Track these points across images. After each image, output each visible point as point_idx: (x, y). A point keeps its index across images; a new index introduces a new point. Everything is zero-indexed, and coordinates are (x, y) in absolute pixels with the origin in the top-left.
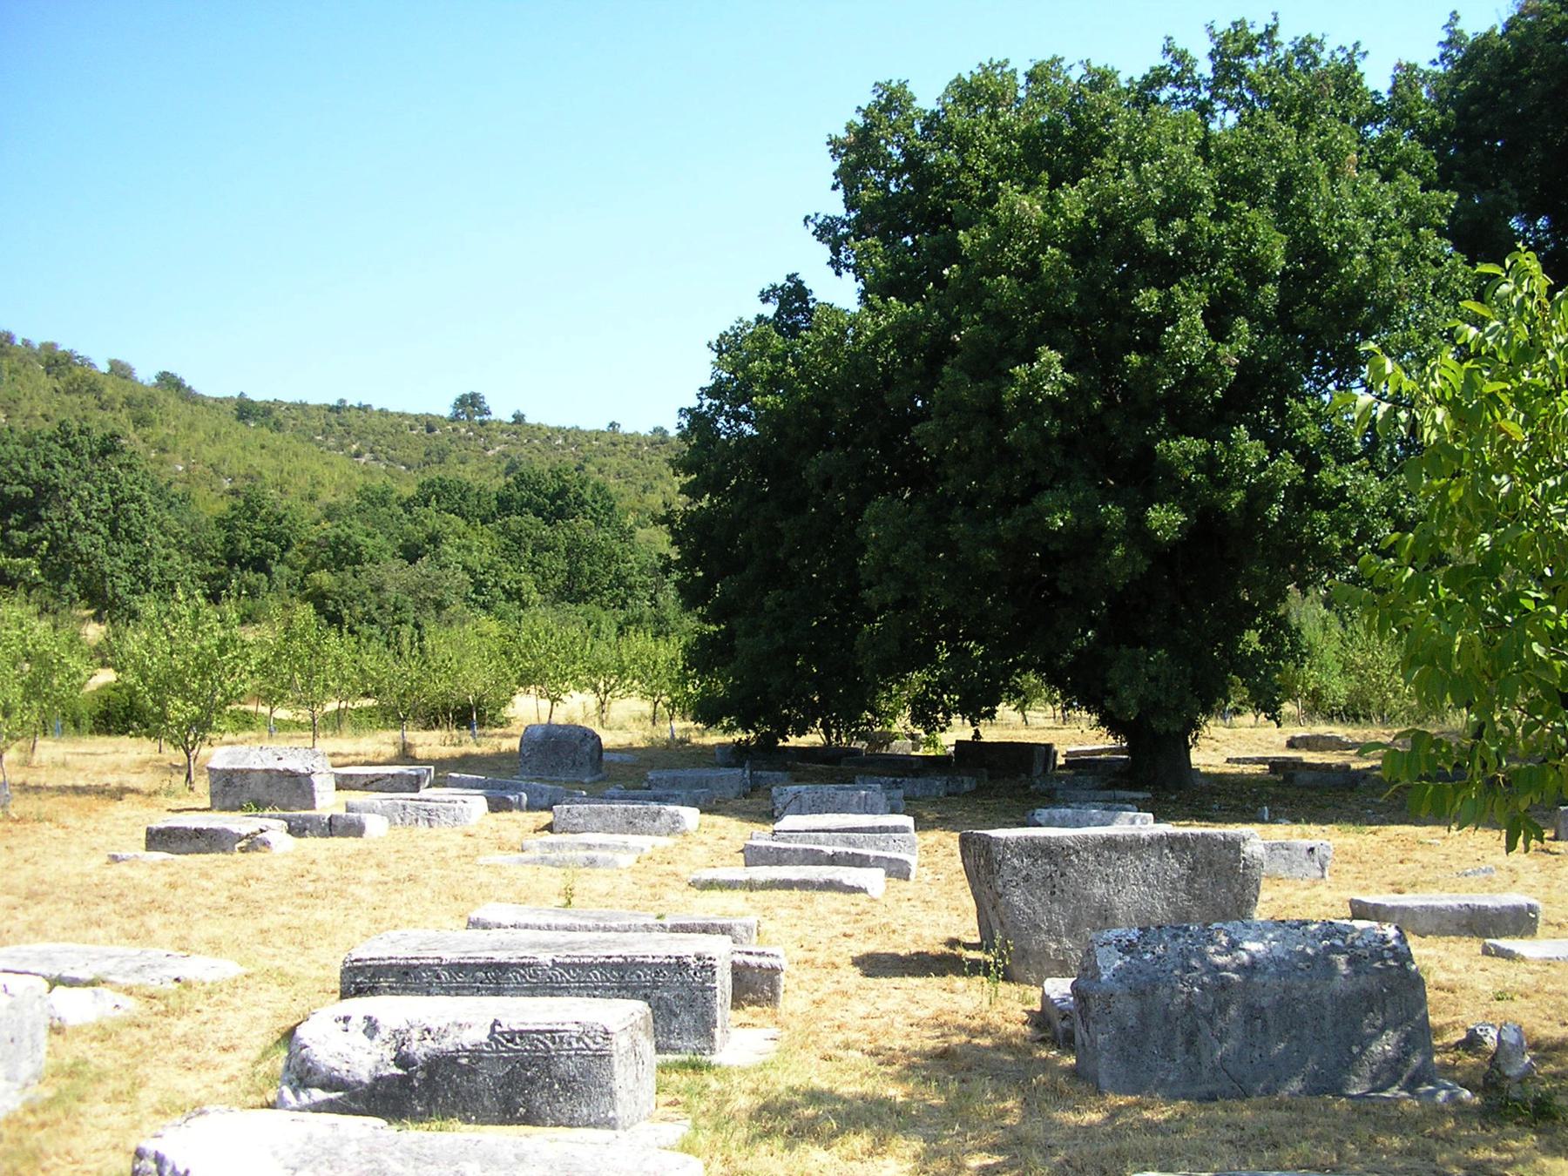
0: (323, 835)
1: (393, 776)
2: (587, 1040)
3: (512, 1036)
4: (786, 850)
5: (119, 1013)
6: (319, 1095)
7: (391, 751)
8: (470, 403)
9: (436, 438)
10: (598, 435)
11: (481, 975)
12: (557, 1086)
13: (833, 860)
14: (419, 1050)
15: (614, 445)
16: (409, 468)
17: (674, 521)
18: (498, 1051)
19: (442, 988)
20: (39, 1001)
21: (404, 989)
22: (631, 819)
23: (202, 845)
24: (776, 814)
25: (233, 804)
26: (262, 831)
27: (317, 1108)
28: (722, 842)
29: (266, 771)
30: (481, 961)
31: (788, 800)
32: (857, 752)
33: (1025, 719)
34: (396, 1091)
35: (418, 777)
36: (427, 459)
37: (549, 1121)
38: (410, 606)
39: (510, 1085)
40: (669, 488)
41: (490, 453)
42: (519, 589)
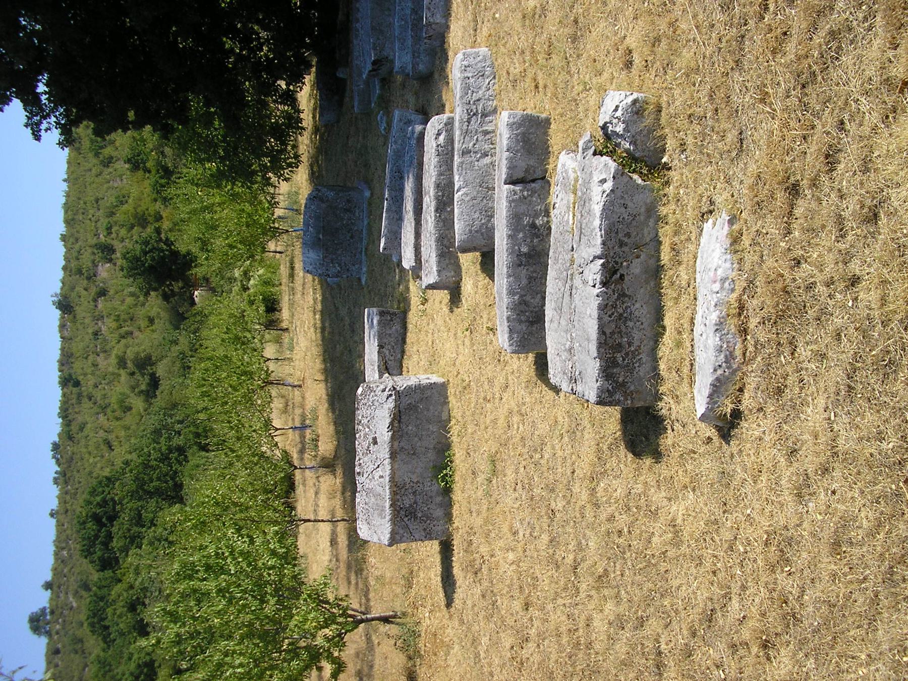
1: (381, 346)
7: (331, 482)
8: (37, 623)
9: (64, 647)
10: (60, 525)
15: (67, 511)
25: (441, 505)
29: (393, 455)
36: (80, 653)
40: (99, 465)
41: (75, 604)
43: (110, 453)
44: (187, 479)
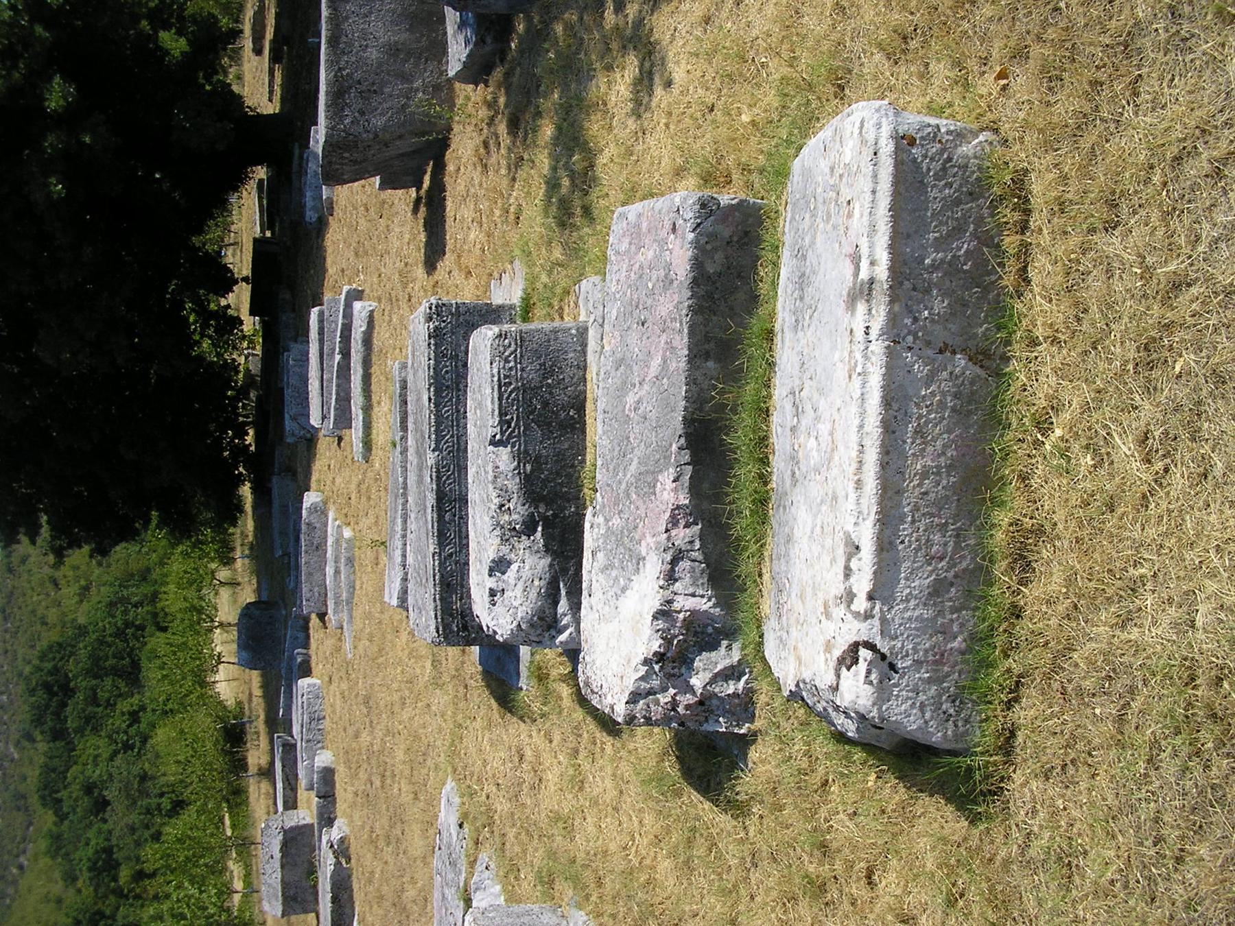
0: (334, 802)
2: (506, 354)
3: (504, 423)
4: (337, 394)
5: (492, 866)
6: (563, 607)
7: (265, 786)
11: (447, 516)
12: (550, 381)
13: (346, 354)
14: (518, 511)
15: (6, 652)
16: (31, 824)
17: (60, 545)
18: (519, 436)
19: (460, 551)
20: (487, 914)
21: (462, 586)
22: (314, 548)
23: (346, 896)
24: (309, 436)
26: (332, 846)
27: (576, 607)
28: (332, 467)
29: (282, 867)
30: (435, 516)
31: (297, 426)
32: (258, 398)
33: (232, 244)
34: (557, 531)
35: (284, 746)
37: (581, 387)
38: (146, 802)
39: (549, 424)
40: (43, 603)
41: (16, 756)
42: (130, 713)
43: (56, 592)
44: (146, 661)
